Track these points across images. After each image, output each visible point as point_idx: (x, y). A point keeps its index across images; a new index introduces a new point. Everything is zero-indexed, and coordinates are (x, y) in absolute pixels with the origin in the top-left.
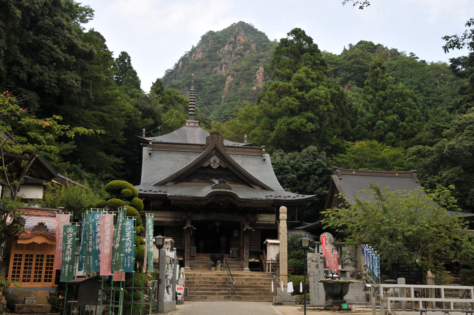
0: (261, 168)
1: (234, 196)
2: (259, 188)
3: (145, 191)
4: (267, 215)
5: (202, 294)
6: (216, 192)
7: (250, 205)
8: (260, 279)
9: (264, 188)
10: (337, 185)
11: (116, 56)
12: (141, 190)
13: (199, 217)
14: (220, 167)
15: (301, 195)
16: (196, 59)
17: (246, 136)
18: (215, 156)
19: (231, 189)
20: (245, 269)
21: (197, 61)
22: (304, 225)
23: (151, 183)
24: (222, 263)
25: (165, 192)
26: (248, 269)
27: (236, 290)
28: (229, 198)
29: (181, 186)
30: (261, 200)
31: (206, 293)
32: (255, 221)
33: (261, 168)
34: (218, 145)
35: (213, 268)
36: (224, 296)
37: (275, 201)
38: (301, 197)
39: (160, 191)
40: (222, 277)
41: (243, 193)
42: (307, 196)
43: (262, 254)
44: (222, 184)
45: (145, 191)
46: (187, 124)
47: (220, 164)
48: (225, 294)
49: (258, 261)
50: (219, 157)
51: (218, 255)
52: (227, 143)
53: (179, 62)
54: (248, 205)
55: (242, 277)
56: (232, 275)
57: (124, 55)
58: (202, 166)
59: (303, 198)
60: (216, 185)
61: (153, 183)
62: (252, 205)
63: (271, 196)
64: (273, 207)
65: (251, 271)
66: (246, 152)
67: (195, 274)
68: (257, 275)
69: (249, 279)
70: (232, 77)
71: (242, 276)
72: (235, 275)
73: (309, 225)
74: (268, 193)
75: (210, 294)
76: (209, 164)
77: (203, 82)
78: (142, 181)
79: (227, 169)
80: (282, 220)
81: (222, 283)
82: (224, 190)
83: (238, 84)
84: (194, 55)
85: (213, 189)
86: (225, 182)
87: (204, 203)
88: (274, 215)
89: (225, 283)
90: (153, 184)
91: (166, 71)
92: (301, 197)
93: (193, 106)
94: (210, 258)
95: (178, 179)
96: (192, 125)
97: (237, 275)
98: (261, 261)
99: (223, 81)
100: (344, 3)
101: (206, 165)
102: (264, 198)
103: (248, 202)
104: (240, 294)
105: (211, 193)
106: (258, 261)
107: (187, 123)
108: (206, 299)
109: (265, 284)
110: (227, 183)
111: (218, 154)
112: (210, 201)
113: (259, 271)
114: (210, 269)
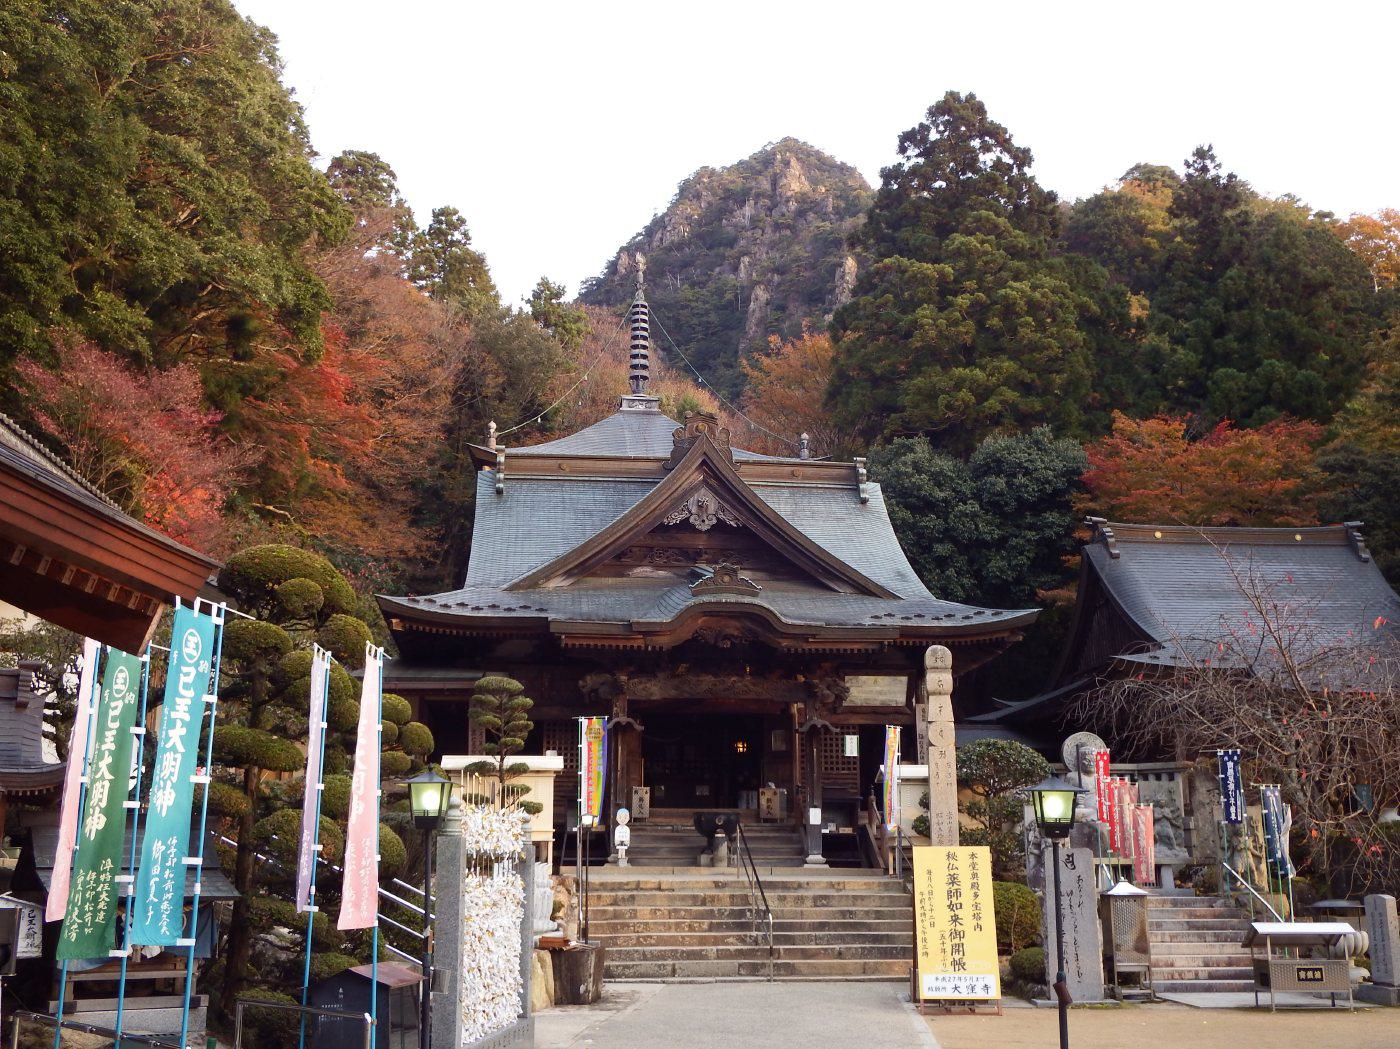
0: (860, 533)
1: (762, 619)
2: (849, 590)
3: (477, 608)
4: (880, 679)
5: (662, 956)
6: (704, 603)
7: (820, 647)
8: (862, 898)
9: (865, 588)
10: (1103, 576)
11: (423, 221)
12: (462, 605)
13: (655, 690)
14: (720, 527)
15: (988, 612)
16: (666, 243)
17: (805, 436)
18: (703, 491)
19: (755, 594)
20: (811, 858)
21: (669, 249)
22: (997, 709)
23: (498, 584)
24: (732, 840)
25: (541, 610)
26: (819, 857)
27: (778, 940)
28: (749, 624)
29: (595, 589)
30: (859, 629)
31: (674, 955)
32: (840, 698)
33: (860, 533)
34: (712, 455)
35: (704, 858)
36: (736, 962)
37: (905, 632)
38: (988, 616)
39: (525, 607)
40: (727, 892)
41: (794, 607)
42: (1008, 615)
43: (866, 806)
44: (727, 578)
45: (477, 608)
46: (625, 407)
47: (721, 516)
48: (740, 954)
49: (848, 830)
50: (716, 493)
51: (721, 815)
52: (739, 455)
53: (618, 257)
54: (813, 647)
55: (800, 893)
56: (760, 885)
57: (446, 221)
58: (662, 524)
59: (995, 619)
60: (705, 583)
61: (505, 581)
62: (828, 647)
63: (890, 615)
64: (902, 654)
65: (832, 864)
66: (805, 477)
67: (638, 883)
68: (856, 883)
69: (826, 897)
70: (766, 289)
71: (800, 886)
72: (772, 885)
73: (1016, 706)
74: (881, 607)
75: (691, 955)
76: (684, 515)
77: (684, 307)
78: (470, 579)
79: (742, 531)
80: (934, 693)
81: (732, 914)
82: (732, 598)
83: (782, 308)
84: (659, 235)
85: (695, 595)
86: (735, 571)
87: (664, 641)
88: (904, 679)
89: (742, 913)
90: (505, 586)
91: (584, 283)
92: (988, 616)
93: (643, 352)
94: (691, 822)
95: (584, 565)
96: (641, 408)
97: (785, 886)
98: (863, 831)
99: (743, 297)
100: (930, 872)
101: (676, 518)
102: (868, 622)
103: (814, 636)
104: (790, 953)
105: (689, 609)
106: (848, 830)
107: (624, 403)
108: (674, 973)
109: (879, 915)
110: (744, 575)
111: (712, 482)
112: (685, 634)
113: (858, 865)
114: (695, 863)
